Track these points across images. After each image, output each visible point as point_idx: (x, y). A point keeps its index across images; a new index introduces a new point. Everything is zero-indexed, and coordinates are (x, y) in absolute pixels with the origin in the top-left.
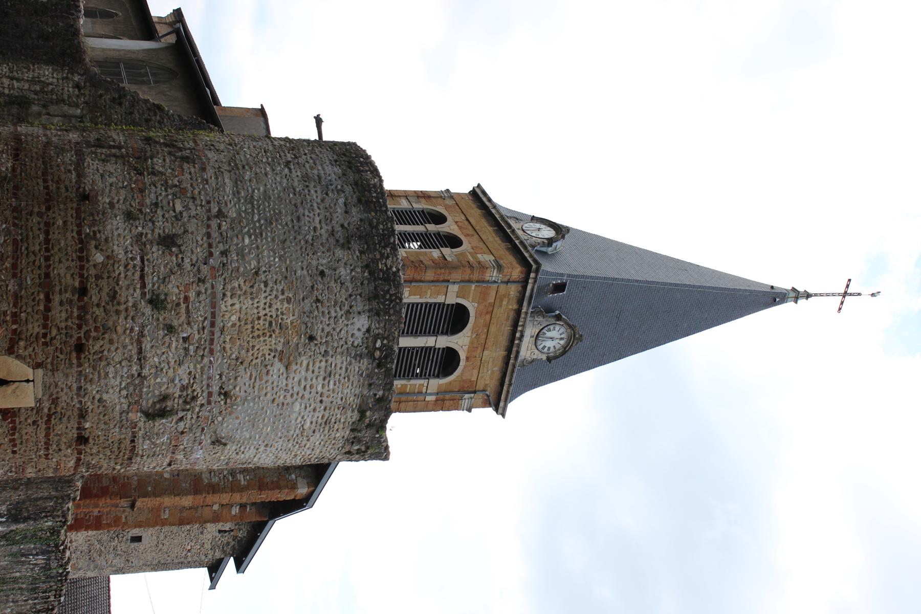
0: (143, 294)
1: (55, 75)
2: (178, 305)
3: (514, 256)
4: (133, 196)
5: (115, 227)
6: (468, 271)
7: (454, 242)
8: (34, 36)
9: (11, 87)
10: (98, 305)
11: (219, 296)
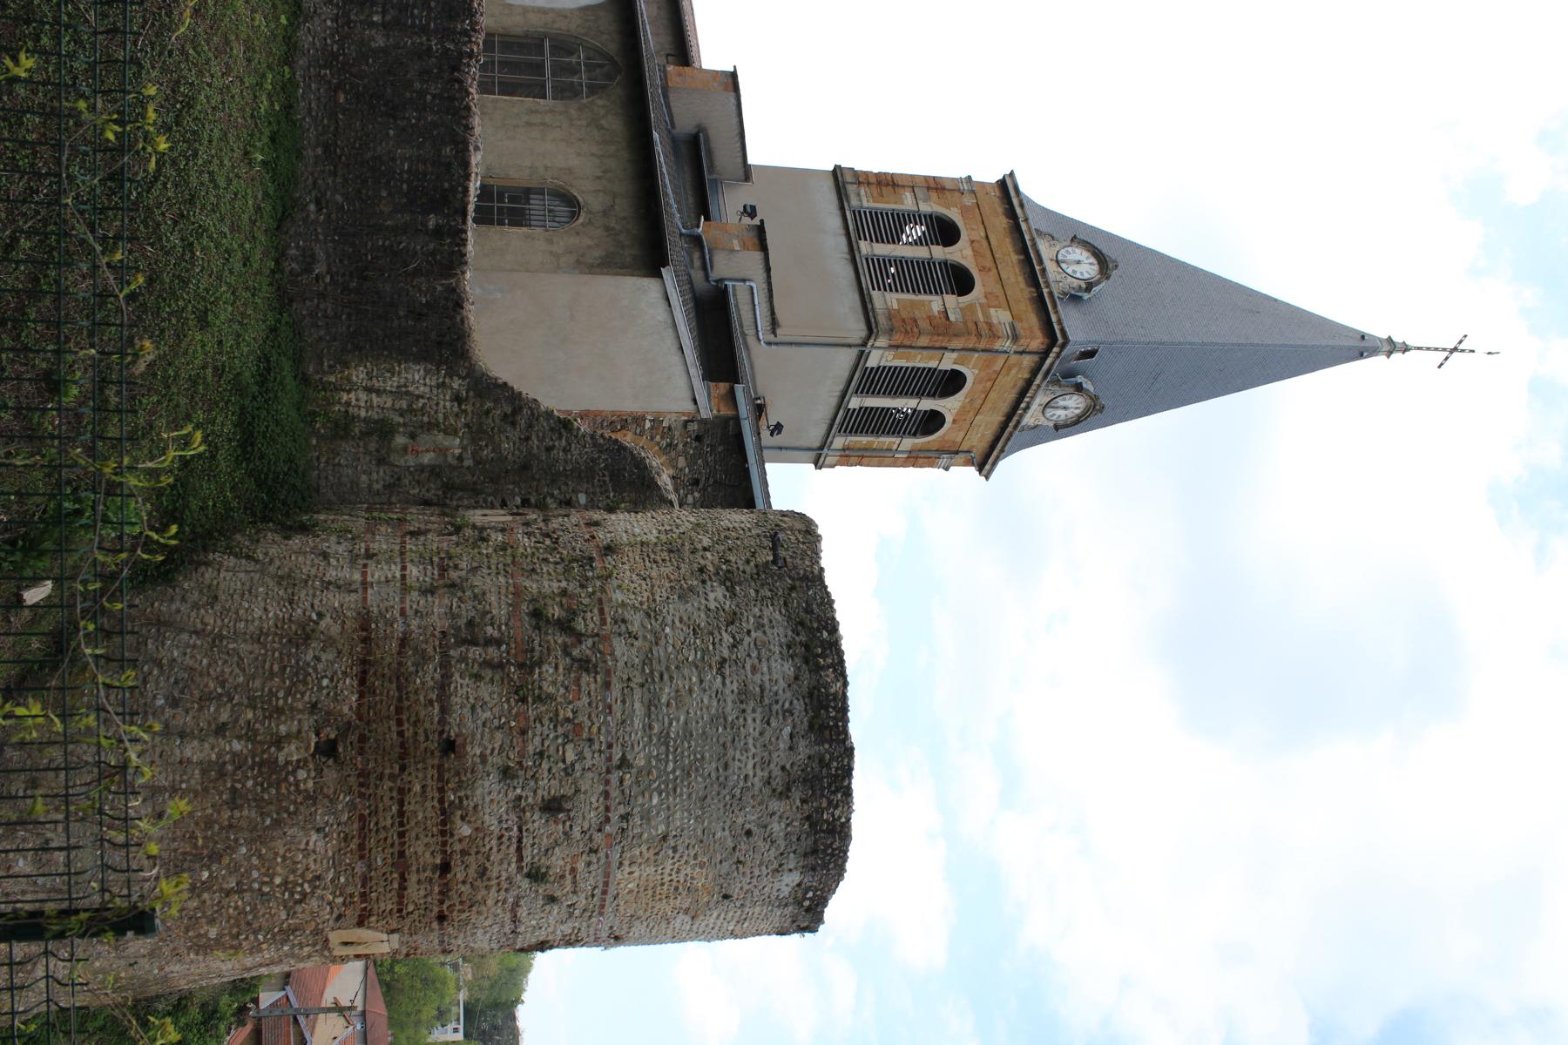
0: (520, 869)
1: (427, 380)
2: (563, 877)
3: (1037, 315)
4: (511, 741)
5: (486, 790)
6: (974, 338)
7: (961, 281)
8: (401, 313)
9: (369, 407)
10: (464, 882)
11: (615, 864)
